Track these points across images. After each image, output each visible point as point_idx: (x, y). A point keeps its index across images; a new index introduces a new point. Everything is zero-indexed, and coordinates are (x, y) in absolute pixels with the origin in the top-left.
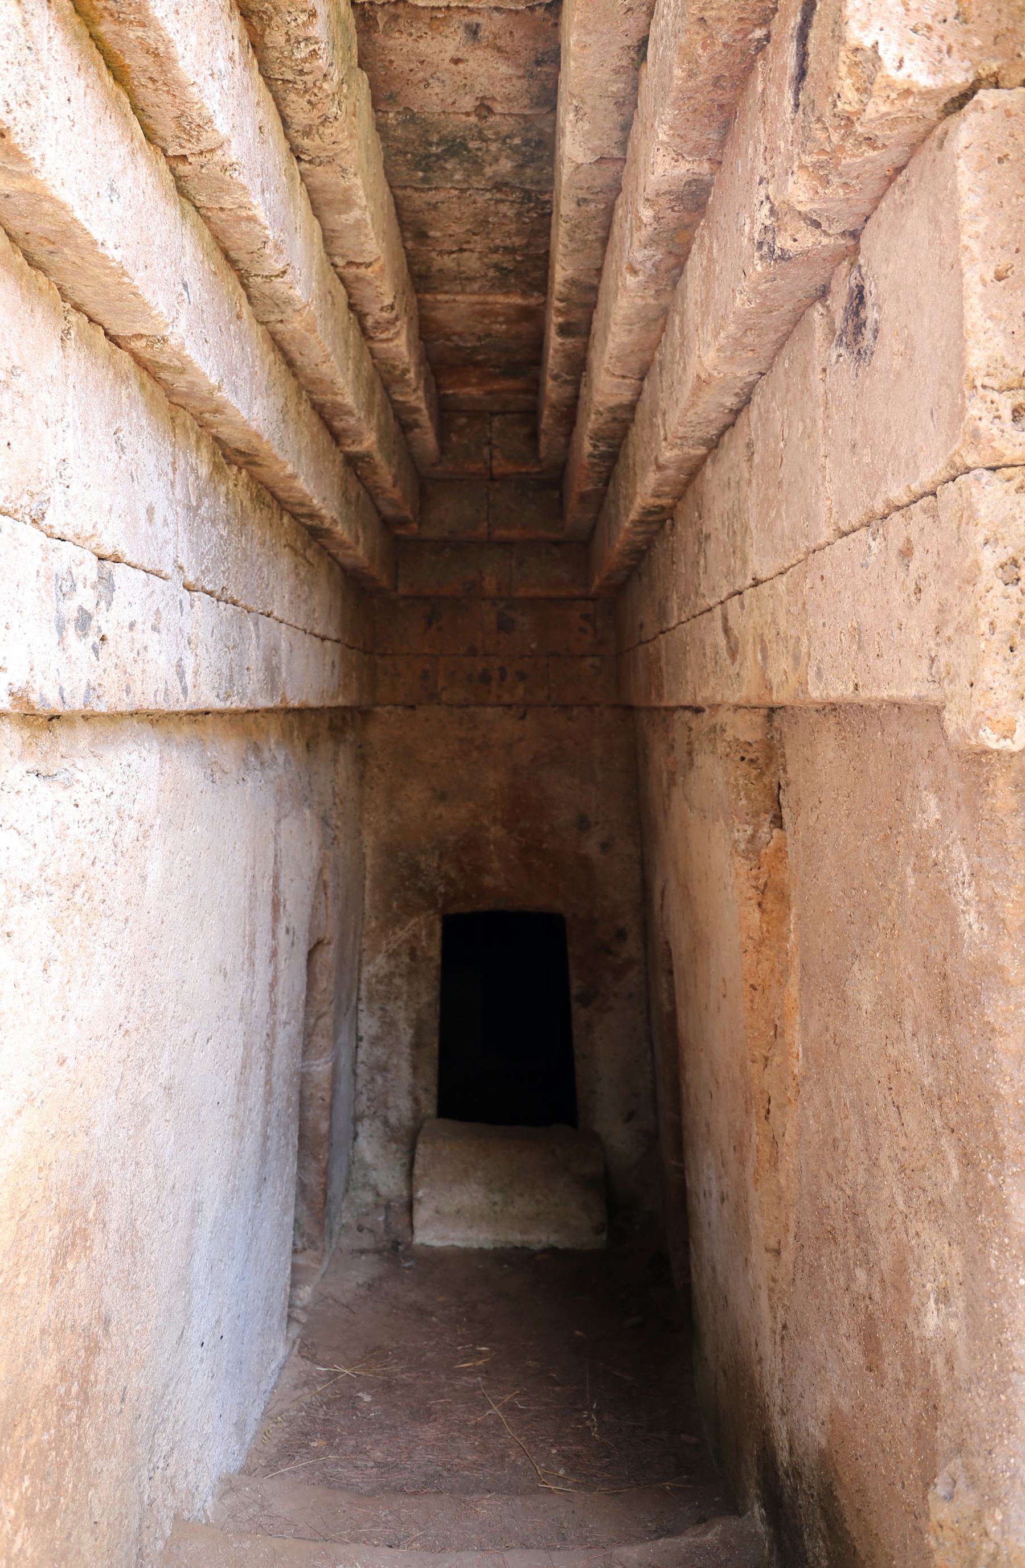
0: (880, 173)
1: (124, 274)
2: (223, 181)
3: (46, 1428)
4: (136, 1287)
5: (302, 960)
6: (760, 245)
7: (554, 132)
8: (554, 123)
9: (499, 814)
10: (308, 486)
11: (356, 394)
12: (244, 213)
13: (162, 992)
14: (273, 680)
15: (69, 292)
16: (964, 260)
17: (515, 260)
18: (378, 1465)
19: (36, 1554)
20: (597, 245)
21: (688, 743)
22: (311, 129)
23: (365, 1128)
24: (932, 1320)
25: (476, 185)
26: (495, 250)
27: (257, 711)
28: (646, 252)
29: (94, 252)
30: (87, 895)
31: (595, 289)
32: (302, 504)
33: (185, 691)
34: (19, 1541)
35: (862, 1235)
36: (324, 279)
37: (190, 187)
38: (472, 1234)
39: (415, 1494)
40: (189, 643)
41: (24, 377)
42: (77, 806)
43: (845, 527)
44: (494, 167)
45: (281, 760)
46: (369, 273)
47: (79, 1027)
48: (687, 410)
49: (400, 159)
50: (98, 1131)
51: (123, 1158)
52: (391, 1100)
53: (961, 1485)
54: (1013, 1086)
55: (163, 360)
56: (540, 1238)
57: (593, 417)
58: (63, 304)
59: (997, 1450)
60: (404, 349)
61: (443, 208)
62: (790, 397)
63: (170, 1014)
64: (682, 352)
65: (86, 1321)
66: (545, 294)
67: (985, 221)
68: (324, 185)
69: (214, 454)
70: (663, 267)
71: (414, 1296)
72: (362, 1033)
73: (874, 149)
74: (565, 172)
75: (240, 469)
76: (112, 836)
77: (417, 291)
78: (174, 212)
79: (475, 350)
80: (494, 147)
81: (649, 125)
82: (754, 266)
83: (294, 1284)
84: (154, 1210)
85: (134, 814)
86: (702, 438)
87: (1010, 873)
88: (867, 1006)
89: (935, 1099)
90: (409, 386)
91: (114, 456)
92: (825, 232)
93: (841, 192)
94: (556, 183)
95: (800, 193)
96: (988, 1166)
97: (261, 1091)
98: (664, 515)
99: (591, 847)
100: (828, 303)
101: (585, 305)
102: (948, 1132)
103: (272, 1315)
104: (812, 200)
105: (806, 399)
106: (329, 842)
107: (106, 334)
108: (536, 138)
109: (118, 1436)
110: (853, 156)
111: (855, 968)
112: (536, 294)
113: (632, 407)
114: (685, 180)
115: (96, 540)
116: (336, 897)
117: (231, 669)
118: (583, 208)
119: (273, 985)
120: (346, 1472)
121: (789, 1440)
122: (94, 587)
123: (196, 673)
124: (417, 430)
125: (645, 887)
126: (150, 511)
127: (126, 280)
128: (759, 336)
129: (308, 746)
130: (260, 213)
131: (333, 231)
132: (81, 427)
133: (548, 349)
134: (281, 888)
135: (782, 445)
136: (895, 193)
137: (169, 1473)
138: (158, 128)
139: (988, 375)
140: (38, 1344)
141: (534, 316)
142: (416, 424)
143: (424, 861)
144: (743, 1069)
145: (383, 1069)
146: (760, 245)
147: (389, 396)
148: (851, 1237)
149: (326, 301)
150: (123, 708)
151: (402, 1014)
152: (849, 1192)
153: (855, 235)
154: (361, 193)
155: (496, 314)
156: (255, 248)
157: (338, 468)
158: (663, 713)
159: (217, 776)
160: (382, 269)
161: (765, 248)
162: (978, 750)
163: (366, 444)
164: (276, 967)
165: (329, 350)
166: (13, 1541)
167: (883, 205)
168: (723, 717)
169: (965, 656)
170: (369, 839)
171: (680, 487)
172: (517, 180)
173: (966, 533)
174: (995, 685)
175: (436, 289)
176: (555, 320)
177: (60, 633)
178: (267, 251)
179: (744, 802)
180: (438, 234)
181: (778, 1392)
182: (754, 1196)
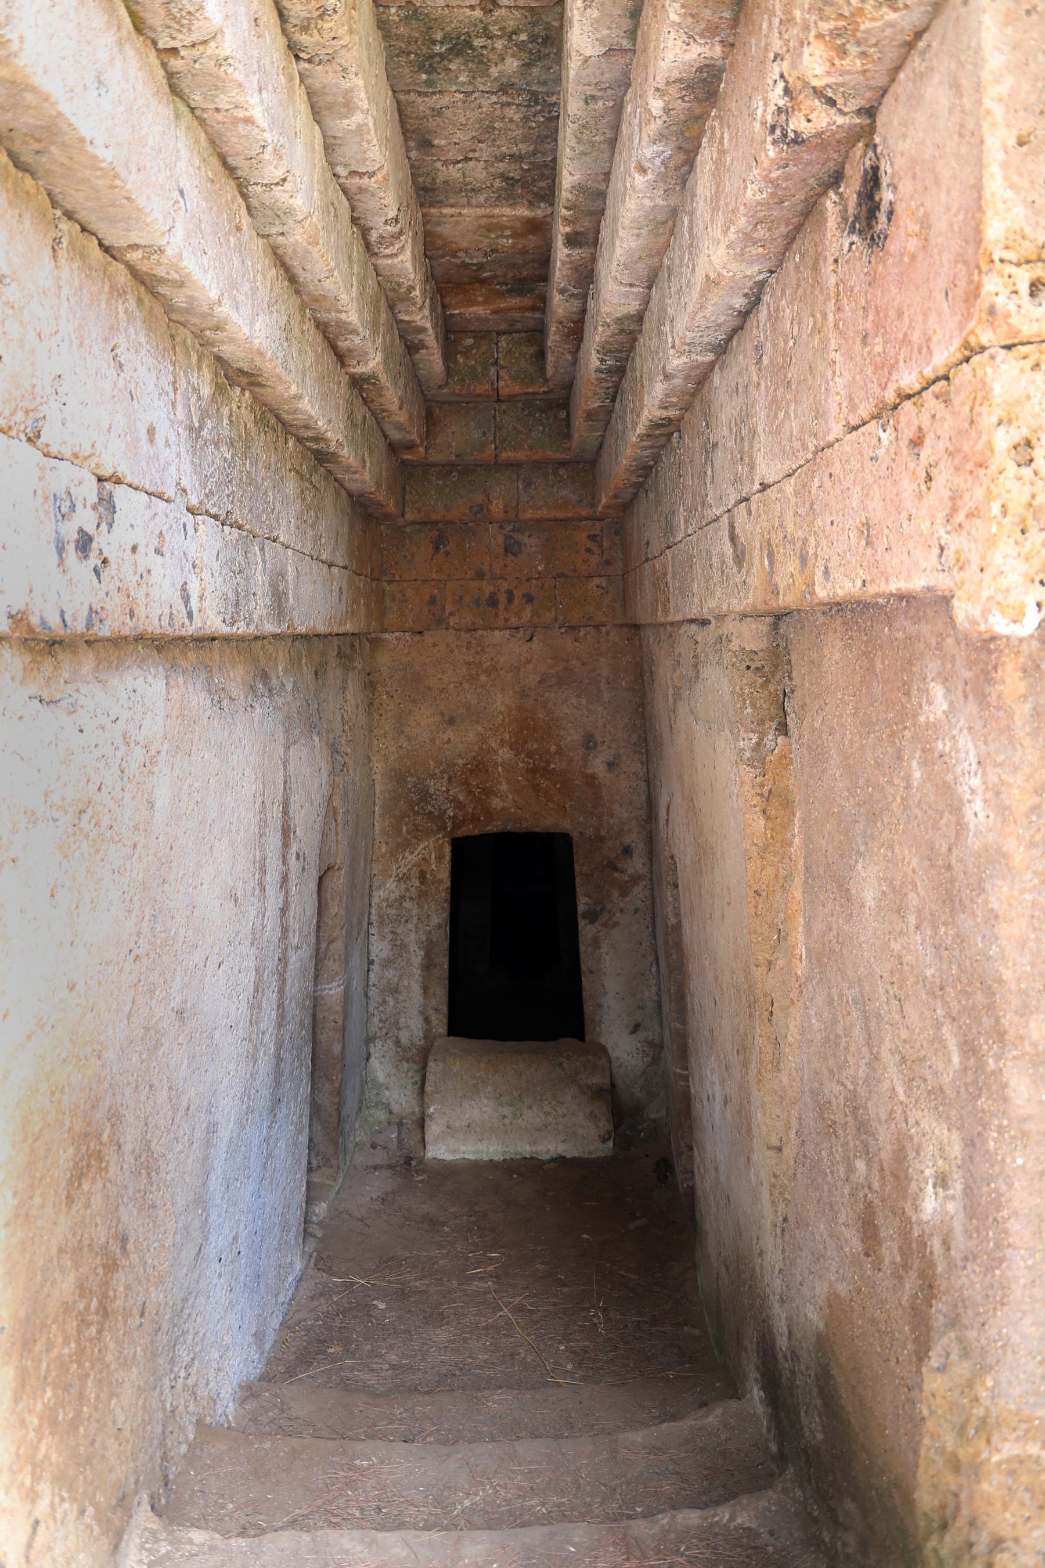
0: (901, 38)
1: (116, 176)
2: (218, 78)
3: (66, 1342)
4: (153, 1206)
5: (313, 886)
6: (773, 129)
7: (562, 27)
8: (561, 16)
9: (507, 736)
10: (313, 407)
11: (361, 312)
12: (240, 114)
13: (172, 918)
14: (280, 606)
15: (59, 197)
16: (985, 128)
17: (521, 168)
18: (393, 1367)
19: (61, 1459)
20: (605, 146)
21: (695, 657)
22: (309, 24)
23: (377, 1049)
24: (930, 1205)
25: (482, 88)
26: (501, 159)
27: (265, 638)
28: (655, 148)
29: (82, 150)
30: (94, 821)
31: (602, 195)
32: (307, 427)
33: (190, 615)
34: (43, 1448)
35: (863, 1127)
36: (327, 188)
37: (183, 84)
38: (482, 1147)
39: (428, 1393)
40: (194, 567)
41: (14, 285)
42: (81, 731)
43: (854, 421)
44: (500, 67)
45: (289, 687)
46: (372, 183)
47: (89, 952)
48: (695, 313)
49: (403, 59)
50: (110, 1055)
51: (137, 1081)
52: (402, 1020)
53: (954, 1357)
54: (1015, 971)
55: (161, 272)
56: (549, 1148)
57: (600, 329)
58: (52, 211)
59: (991, 1322)
60: (409, 265)
61: (448, 113)
62: (800, 291)
63: (181, 939)
64: (690, 253)
65: (103, 1240)
66: (552, 205)
67: (1009, 81)
68: (324, 87)
69: (216, 374)
70: (672, 165)
71: (427, 1208)
72: (373, 957)
73: (895, 10)
74: (573, 66)
75: (243, 390)
76: (118, 761)
77: (422, 205)
78: (168, 112)
79: (481, 267)
80: (499, 44)
81: (659, 7)
82: (766, 151)
83: (309, 1201)
84: (168, 1131)
85: (140, 739)
86: (709, 344)
87: (1016, 759)
88: (870, 903)
89: (937, 989)
90: (415, 304)
91: (112, 373)
92: (840, 110)
93: (858, 63)
94: (564, 82)
95: (816, 66)
96: (989, 1051)
97: (274, 1014)
98: (672, 428)
99: (598, 766)
100: (841, 190)
101: (592, 213)
102: (948, 1020)
103: (288, 1231)
104: (828, 73)
105: (817, 292)
106: (337, 769)
107: (101, 245)
108: (543, 34)
109: (139, 1349)
110: (873, 19)
111: (860, 866)
112: (542, 205)
113: (639, 318)
114: (696, 65)
115: (94, 460)
116: (346, 823)
117: (237, 594)
118: (591, 106)
119: (284, 910)
120: (362, 1375)
121: (788, 1326)
122: (94, 508)
123: (201, 597)
124: (423, 351)
125: (651, 803)
126: (151, 431)
127: (118, 182)
128: (769, 230)
129: (316, 673)
130: (257, 113)
131: (335, 138)
132: (76, 343)
133: (555, 262)
134: (291, 814)
135: (791, 343)
136: (915, 62)
137: (190, 1381)
138: (147, 15)
139: (1007, 248)
140: (55, 1262)
141: (539, 228)
142: (422, 345)
143: (433, 786)
144: (747, 972)
145: (395, 991)
146: (773, 129)
147: (394, 315)
148: (851, 1129)
149: (329, 214)
150: (126, 632)
151: (412, 938)
152: (850, 1087)
153: (870, 112)
154: (363, 95)
155: (503, 228)
156: (254, 153)
157: (344, 389)
158: (669, 629)
159: (225, 703)
160: (386, 179)
161: (778, 132)
162: (986, 636)
163: (371, 364)
164: (287, 893)
165: (332, 264)
166: (37, 1448)
167: (902, 75)
168: (730, 626)
169: (976, 541)
170: (378, 766)
171: (687, 397)
172: (523, 82)
173: (980, 414)
174: (1006, 569)
175: (441, 202)
176: (561, 230)
177: (60, 554)
178: (266, 156)
179: (749, 710)
180: (443, 142)
181: (778, 1282)
182: (757, 1096)
